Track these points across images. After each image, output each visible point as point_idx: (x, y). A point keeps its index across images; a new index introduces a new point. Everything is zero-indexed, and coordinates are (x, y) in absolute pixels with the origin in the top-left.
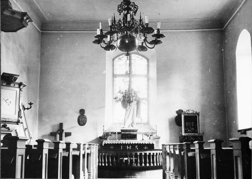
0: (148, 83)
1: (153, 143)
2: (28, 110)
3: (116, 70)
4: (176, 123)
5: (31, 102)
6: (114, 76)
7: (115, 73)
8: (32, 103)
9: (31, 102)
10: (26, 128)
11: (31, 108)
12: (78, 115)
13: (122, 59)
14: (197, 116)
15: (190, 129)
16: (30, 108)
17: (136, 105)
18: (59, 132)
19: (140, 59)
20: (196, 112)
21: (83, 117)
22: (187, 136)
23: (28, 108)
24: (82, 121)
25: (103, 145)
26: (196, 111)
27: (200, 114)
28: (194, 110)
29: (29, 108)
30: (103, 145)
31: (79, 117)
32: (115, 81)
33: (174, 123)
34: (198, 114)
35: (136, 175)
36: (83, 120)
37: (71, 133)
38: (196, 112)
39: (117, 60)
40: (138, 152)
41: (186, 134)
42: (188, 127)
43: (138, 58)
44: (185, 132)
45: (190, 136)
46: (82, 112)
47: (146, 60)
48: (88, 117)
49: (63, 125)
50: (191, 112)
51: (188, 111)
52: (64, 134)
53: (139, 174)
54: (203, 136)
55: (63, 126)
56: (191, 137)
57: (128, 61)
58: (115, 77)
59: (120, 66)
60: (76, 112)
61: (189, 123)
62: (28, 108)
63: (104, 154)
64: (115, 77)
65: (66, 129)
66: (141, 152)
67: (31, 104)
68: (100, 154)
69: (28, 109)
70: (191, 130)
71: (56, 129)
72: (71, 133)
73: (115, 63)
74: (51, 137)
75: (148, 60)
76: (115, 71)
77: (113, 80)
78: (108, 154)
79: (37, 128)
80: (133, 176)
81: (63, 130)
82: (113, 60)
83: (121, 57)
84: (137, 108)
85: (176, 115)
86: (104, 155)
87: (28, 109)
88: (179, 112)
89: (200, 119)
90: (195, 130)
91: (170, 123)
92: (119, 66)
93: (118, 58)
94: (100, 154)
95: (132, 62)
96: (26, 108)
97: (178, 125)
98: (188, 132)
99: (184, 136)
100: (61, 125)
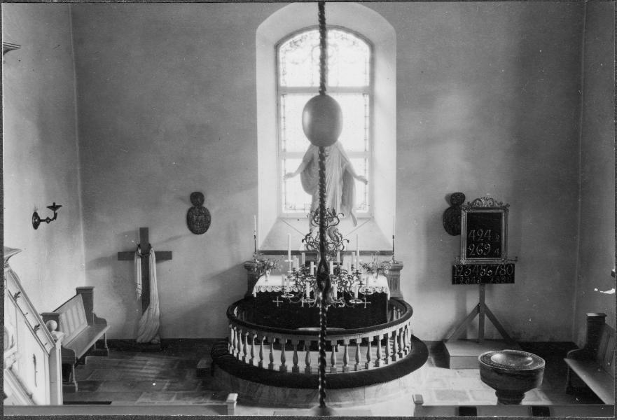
0: (372, 112)
1: (384, 291)
2: (48, 223)
3: (283, 75)
4: (445, 228)
5: (54, 204)
6: (280, 91)
7: (282, 84)
8: (56, 204)
9: (54, 204)
10: (39, 325)
11: (55, 218)
12: (188, 206)
13: (302, 44)
14: (500, 214)
15: (483, 248)
16: (53, 220)
17: (340, 182)
18: (140, 251)
19: (351, 43)
20: (501, 203)
21: (201, 214)
22: (472, 266)
23: (48, 218)
24: (198, 220)
25: (255, 296)
26: (499, 202)
27: (509, 208)
28: (496, 199)
29: (51, 217)
30: (255, 296)
31: (190, 210)
32: (282, 107)
33: (441, 223)
34: (505, 209)
35: (339, 401)
36: (201, 220)
37: (171, 259)
38: (501, 203)
39: (285, 46)
40: (344, 338)
41: (472, 261)
42: (477, 243)
43: (345, 40)
44: (468, 256)
45: (480, 266)
46: (197, 199)
47: (366, 48)
48: (212, 212)
49: (149, 232)
50: (485, 204)
51: (478, 201)
52: (153, 257)
53: (348, 396)
54: (514, 265)
55: (150, 235)
56: (484, 268)
57: (318, 52)
58: (283, 95)
59: (297, 64)
60: (182, 199)
61: (480, 233)
62: (48, 218)
63: (256, 336)
64: (283, 95)
65: (157, 241)
66: (352, 338)
67: (54, 207)
68: (247, 334)
69: (48, 220)
70: (484, 250)
71: (133, 242)
72: (171, 259)
73: (281, 55)
74: (121, 262)
75: (372, 47)
76: (281, 78)
77: (278, 105)
78: (266, 338)
79: (82, 241)
80: (332, 401)
81: (150, 247)
82: (277, 47)
83: (297, 37)
84: (344, 190)
85: (447, 206)
86: (256, 339)
87: (48, 220)
88: (456, 200)
89: (510, 224)
90: (496, 248)
91: (429, 231)
92: (293, 63)
93: (291, 40)
94: (247, 334)
95: (330, 51)
96: (41, 219)
97: (450, 233)
98: (477, 256)
99: (464, 266)
100: (144, 233)
